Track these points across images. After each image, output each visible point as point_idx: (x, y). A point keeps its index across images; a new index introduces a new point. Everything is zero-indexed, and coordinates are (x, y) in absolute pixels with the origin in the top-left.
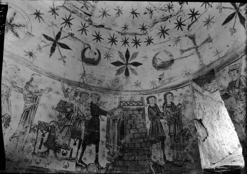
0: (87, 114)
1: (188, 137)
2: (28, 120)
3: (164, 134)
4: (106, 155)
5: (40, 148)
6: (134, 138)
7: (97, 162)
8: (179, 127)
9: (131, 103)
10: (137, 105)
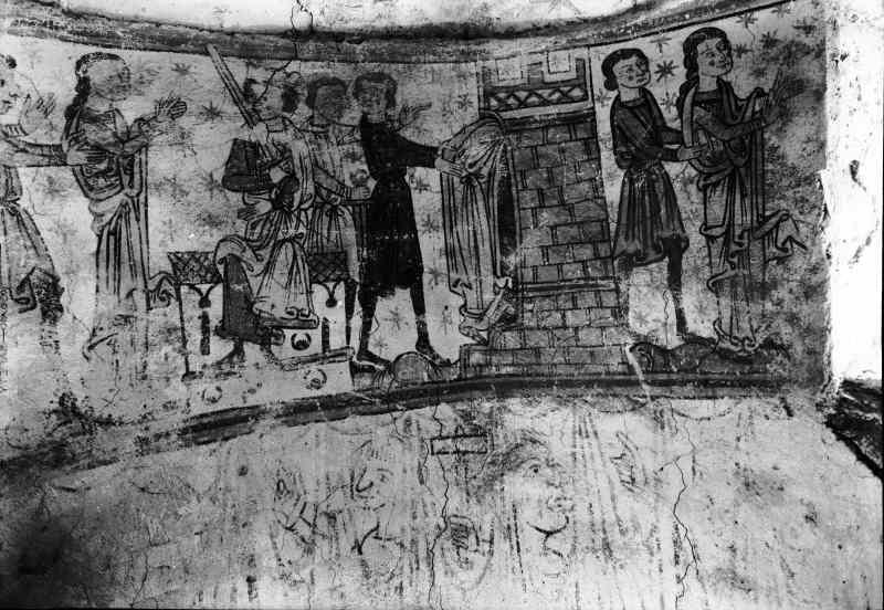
0: (352, 176)
2: (125, 269)
3: (684, 231)
4: (457, 318)
5: (205, 350)
7: (424, 347)
8: (747, 201)
9: (531, 93)
10: (559, 102)
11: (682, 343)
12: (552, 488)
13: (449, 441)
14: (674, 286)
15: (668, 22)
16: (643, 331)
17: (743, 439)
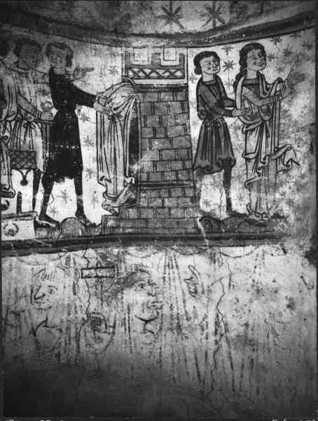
0: (42, 104)
1: (289, 166)
3: (233, 155)
4: (101, 199)
6: (161, 160)
8: (269, 140)
10: (168, 78)
11: (228, 216)
12: (150, 296)
13: (93, 270)
14: (226, 186)
15: (233, 38)
16: (207, 210)
17: (257, 267)
